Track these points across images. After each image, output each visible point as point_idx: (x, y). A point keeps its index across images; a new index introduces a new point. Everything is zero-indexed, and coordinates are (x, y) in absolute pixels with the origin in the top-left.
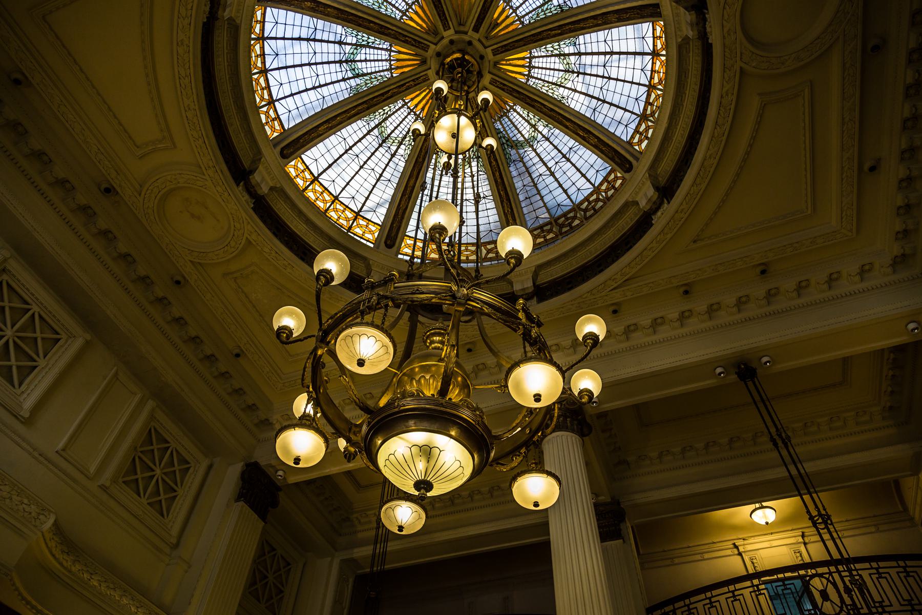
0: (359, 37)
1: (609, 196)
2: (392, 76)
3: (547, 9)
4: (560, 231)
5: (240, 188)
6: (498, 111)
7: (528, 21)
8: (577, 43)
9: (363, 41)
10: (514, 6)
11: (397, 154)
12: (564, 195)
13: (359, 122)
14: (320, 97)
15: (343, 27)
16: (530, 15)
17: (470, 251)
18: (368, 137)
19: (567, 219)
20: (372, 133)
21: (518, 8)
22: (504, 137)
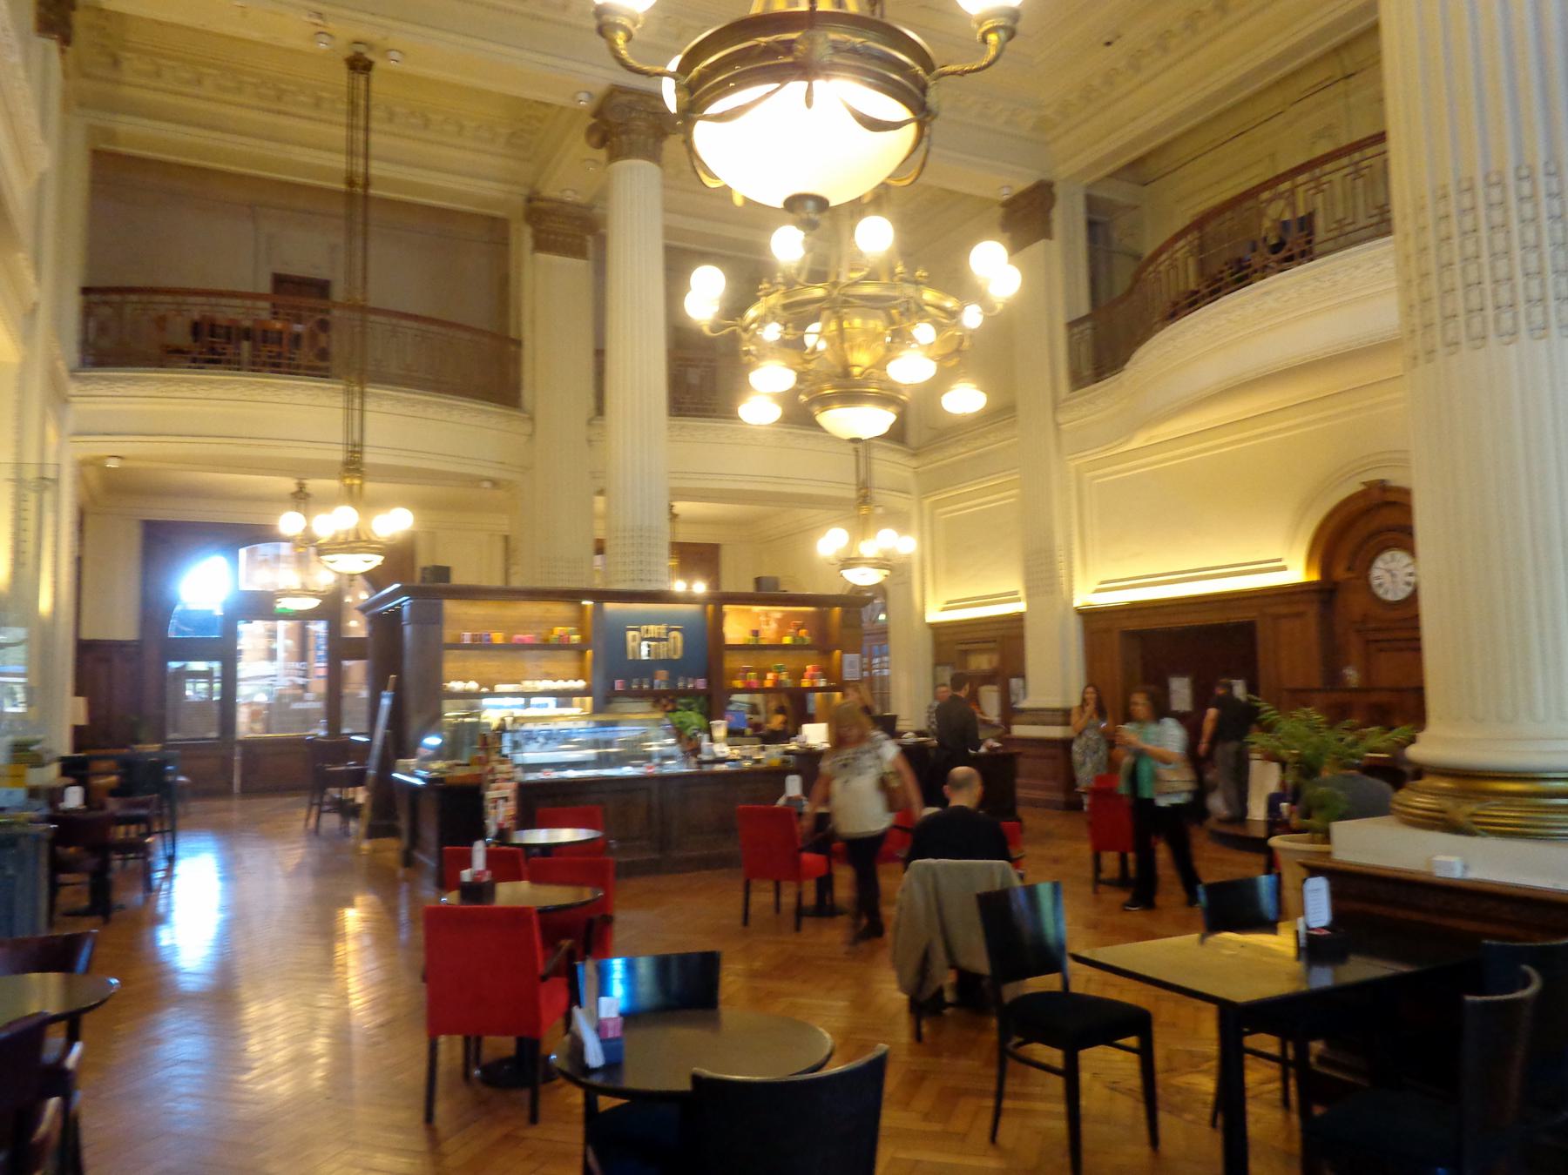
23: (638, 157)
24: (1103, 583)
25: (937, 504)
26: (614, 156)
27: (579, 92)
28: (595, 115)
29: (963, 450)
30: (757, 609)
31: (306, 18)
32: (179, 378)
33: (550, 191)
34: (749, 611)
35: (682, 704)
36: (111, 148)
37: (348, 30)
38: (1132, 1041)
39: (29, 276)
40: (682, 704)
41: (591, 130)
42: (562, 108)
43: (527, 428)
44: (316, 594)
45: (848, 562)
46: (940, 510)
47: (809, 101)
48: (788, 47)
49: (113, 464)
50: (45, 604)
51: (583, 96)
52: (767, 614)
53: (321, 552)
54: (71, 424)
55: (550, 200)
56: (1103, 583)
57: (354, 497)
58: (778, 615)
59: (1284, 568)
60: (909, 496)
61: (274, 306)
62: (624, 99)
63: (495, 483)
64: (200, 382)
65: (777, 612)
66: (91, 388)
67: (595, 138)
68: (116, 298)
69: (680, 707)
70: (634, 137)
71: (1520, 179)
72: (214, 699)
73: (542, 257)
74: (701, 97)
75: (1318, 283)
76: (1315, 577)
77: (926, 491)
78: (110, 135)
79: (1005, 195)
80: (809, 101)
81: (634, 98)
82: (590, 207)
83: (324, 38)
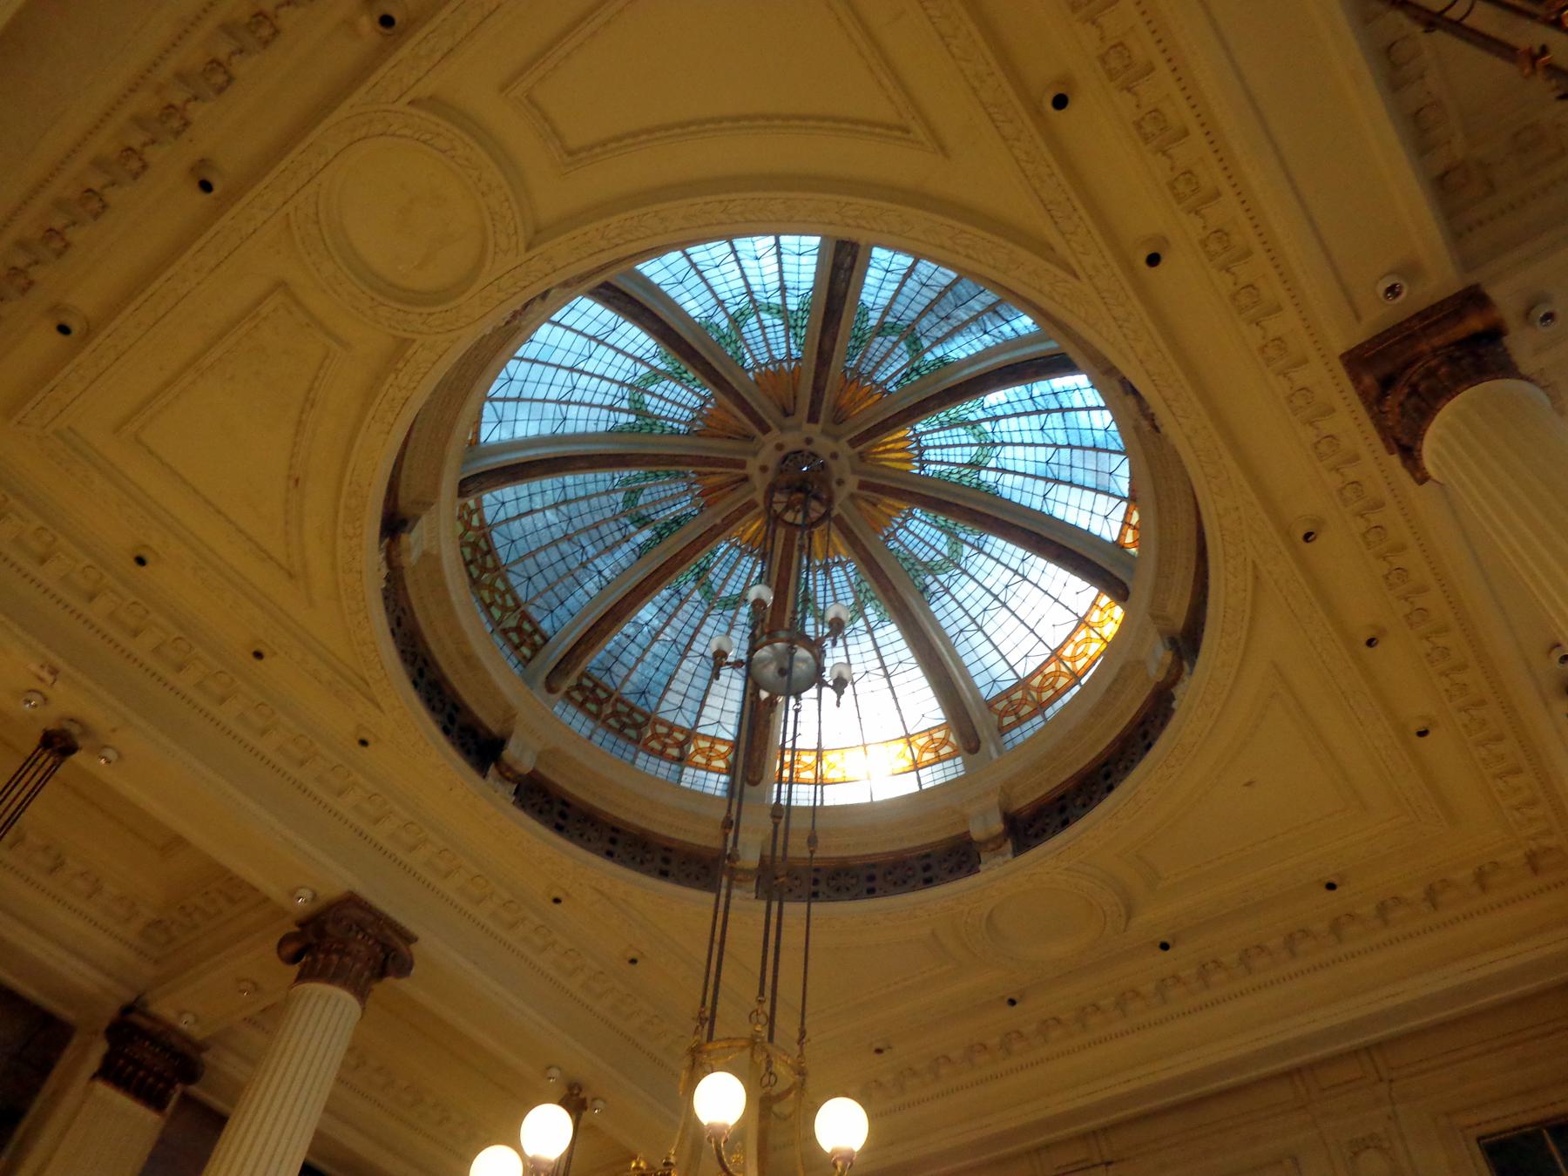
0: (800, 313)
1: (695, 759)
2: (748, 371)
3: (917, 570)
4: (608, 717)
5: (490, 779)
6: (746, 537)
7: (892, 547)
8: (884, 623)
9: (796, 320)
10: (908, 525)
11: (617, 413)
12: (583, 408)
13: (652, 342)
14: (680, 278)
15: (811, 290)
16: (901, 549)
17: (504, 600)
18: (630, 361)
19: (629, 715)
20: (638, 365)
21: (906, 529)
22: (708, 562)
26: (302, 977)
27: (302, 887)
28: (302, 924)
31: (34, 667)
33: (165, 1008)
42: (267, 899)
51: (307, 894)
53: (802, 1054)
55: (154, 1019)
67: (291, 948)
70: (347, 960)
72: (810, 621)
73: (103, 1090)
82: (200, 1047)
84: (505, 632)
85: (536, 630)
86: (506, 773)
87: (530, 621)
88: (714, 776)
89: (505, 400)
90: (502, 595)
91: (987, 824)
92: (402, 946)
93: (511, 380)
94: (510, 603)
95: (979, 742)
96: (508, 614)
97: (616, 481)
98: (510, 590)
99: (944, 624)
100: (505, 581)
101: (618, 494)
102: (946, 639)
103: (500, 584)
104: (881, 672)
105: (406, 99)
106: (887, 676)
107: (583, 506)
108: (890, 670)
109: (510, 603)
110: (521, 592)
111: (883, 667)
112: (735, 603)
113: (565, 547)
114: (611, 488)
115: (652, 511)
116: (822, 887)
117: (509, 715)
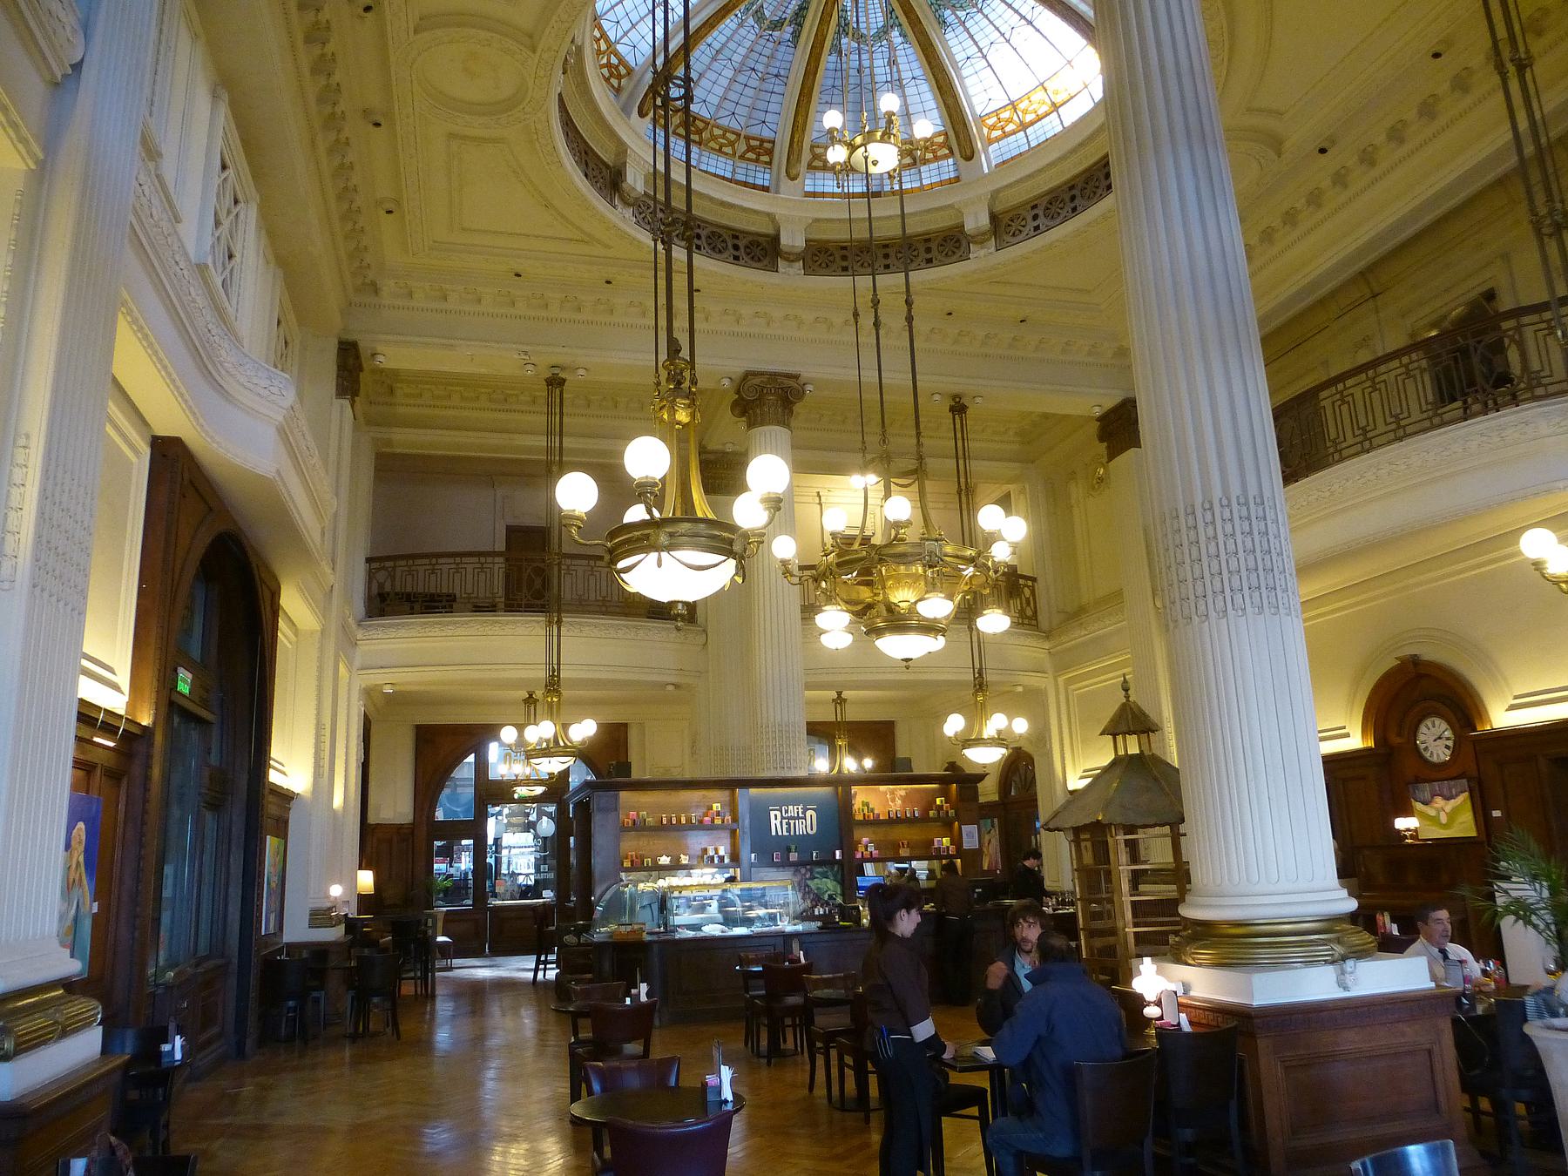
23: (769, 424)
24: (1516, 697)
25: (1069, 682)
26: (751, 425)
29: (1083, 632)
30: (882, 788)
32: (433, 622)
34: (876, 790)
35: (818, 873)
36: (388, 450)
37: (547, 357)
38: (974, 1111)
39: (328, 570)
40: (818, 873)
41: (735, 405)
42: (714, 390)
43: (702, 639)
44: (539, 782)
45: (968, 741)
46: (1073, 687)
47: (659, 564)
48: (647, 537)
49: (388, 690)
50: (338, 801)
52: (892, 793)
54: (358, 662)
56: (1516, 697)
57: (552, 712)
58: (903, 793)
59: (1347, 735)
60: (1046, 675)
61: (507, 560)
62: (757, 381)
63: (677, 686)
64: (448, 624)
65: (901, 790)
66: (373, 633)
67: (737, 412)
68: (389, 564)
69: (816, 875)
71: (1205, 510)
74: (617, 556)
75: (1320, 493)
76: (1371, 743)
77: (1060, 668)
78: (389, 443)
79: (1097, 412)
80: (659, 564)
81: (764, 379)
83: (530, 367)
84: (742, 157)
85: (762, 141)
86: (791, 258)
87: (754, 139)
88: (944, 163)
89: (626, 34)
90: (723, 136)
91: (977, 220)
92: (791, 383)
93: (618, 22)
94: (732, 137)
95: (973, 153)
96: (736, 145)
97: (739, 15)
98: (726, 130)
99: (954, 50)
100: (718, 127)
101: (748, 21)
102: (954, 63)
103: (717, 132)
104: (1023, 22)
105: (411, 33)
106: (1030, 23)
107: (732, 45)
108: (1029, 17)
109: (732, 137)
110: (734, 125)
111: (1024, 17)
112: (885, 33)
113: (742, 78)
114: (740, 21)
115: (780, 13)
116: (1041, 221)
117: (771, 217)
